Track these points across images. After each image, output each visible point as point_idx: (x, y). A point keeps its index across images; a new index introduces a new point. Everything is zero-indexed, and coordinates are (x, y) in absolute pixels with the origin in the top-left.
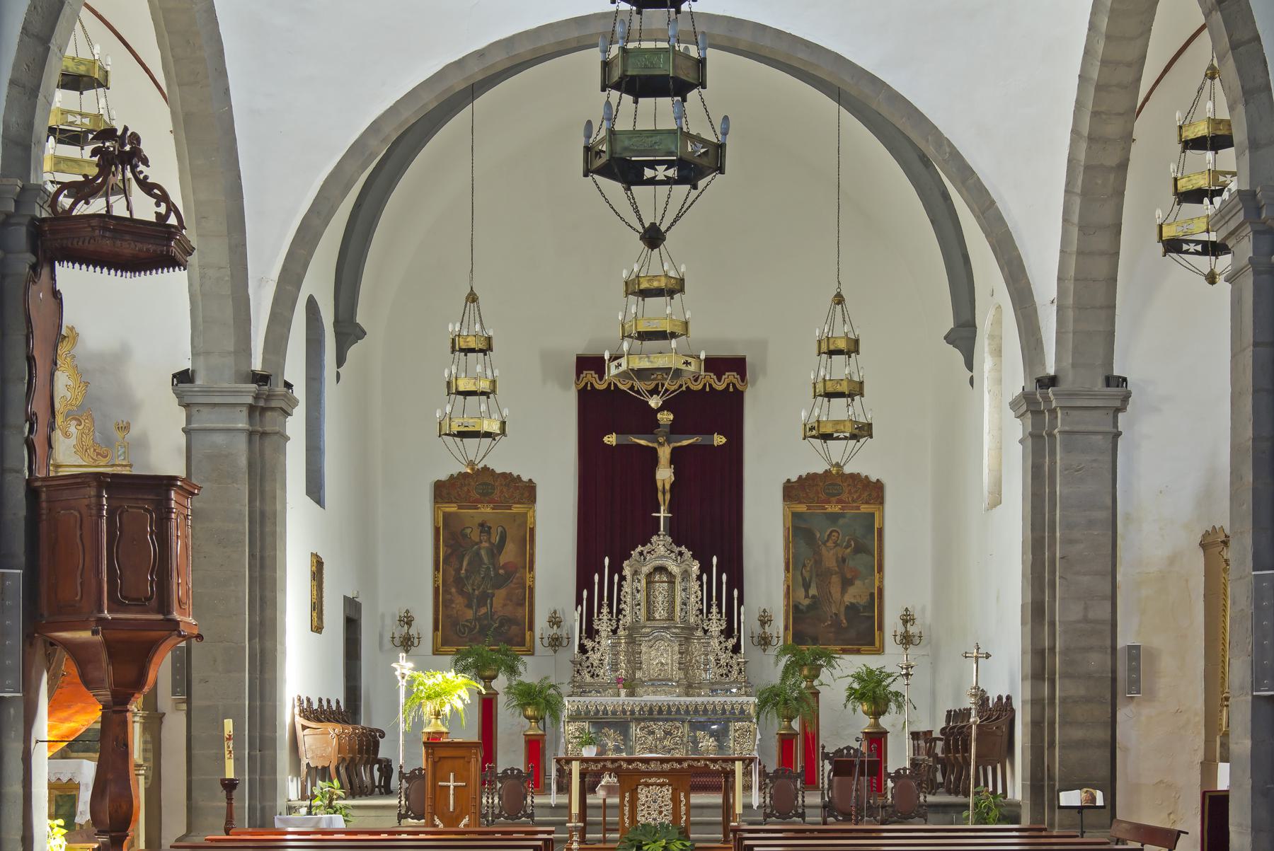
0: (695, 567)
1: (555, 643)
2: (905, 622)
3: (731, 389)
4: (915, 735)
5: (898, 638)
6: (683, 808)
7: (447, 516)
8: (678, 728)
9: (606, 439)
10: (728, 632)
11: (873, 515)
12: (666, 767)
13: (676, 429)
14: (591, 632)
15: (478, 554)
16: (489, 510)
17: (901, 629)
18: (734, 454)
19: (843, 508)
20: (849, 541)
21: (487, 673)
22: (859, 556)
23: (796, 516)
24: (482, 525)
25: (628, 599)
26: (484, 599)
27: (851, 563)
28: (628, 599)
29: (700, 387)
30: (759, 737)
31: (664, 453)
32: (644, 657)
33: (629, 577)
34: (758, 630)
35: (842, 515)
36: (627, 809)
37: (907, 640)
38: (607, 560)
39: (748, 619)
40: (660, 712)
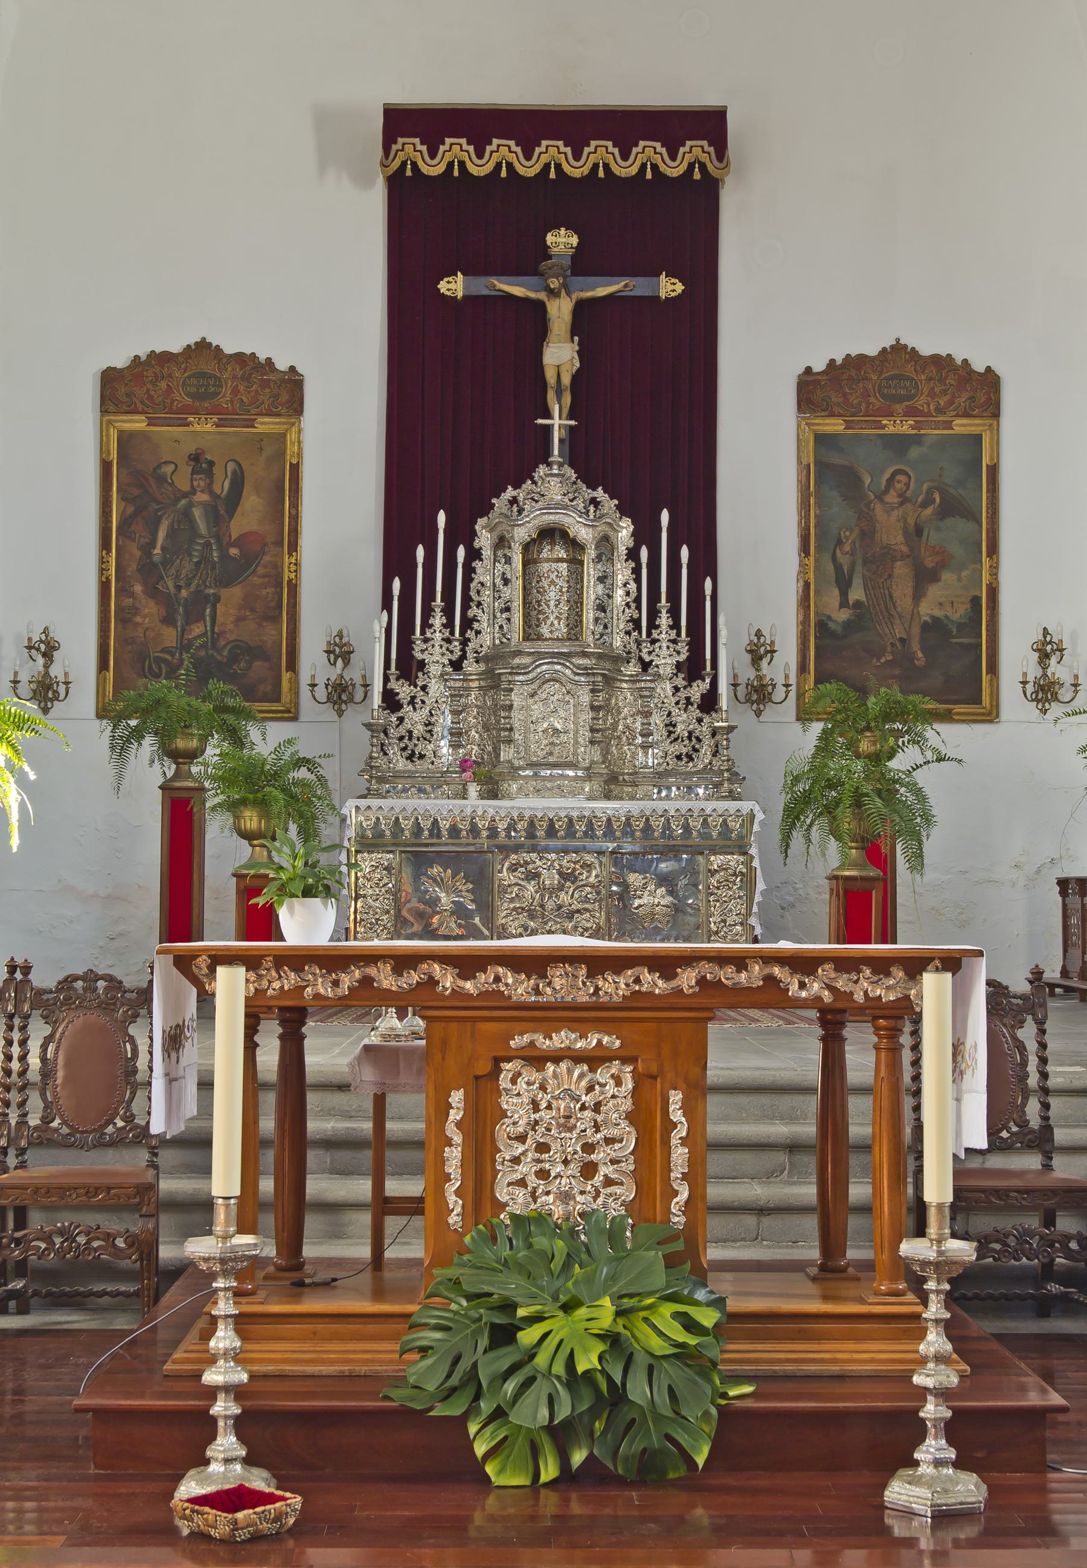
0: (625, 531)
1: (340, 695)
2: (1044, 657)
3: (697, 175)
4: (1063, 884)
5: (1030, 688)
6: (679, 1155)
7: (126, 440)
8: (588, 867)
9: (443, 286)
10: (693, 667)
11: (977, 439)
12: (614, 987)
13: (583, 264)
14: (408, 666)
15: (187, 514)
16: (209, 427)
17: (1034, 672)
18: (695, 323)
19: (917, 426)
20: (930, 491)
21: (181, 744)
22: (950, 521)
23: (822, 440)
24: (196, 458)
26: (200, 605)
27: (933, 537)
28: (487, 596)
29: (634, 170)
30: (761, 886)
32: (517, 717)
33: (487, 553)
34: (748, 674)
35: (916, 440)
36: (454, 1156)
37: (1045, 692)
38: (442, 518)
39: (729, 662)
40: (551, 832)
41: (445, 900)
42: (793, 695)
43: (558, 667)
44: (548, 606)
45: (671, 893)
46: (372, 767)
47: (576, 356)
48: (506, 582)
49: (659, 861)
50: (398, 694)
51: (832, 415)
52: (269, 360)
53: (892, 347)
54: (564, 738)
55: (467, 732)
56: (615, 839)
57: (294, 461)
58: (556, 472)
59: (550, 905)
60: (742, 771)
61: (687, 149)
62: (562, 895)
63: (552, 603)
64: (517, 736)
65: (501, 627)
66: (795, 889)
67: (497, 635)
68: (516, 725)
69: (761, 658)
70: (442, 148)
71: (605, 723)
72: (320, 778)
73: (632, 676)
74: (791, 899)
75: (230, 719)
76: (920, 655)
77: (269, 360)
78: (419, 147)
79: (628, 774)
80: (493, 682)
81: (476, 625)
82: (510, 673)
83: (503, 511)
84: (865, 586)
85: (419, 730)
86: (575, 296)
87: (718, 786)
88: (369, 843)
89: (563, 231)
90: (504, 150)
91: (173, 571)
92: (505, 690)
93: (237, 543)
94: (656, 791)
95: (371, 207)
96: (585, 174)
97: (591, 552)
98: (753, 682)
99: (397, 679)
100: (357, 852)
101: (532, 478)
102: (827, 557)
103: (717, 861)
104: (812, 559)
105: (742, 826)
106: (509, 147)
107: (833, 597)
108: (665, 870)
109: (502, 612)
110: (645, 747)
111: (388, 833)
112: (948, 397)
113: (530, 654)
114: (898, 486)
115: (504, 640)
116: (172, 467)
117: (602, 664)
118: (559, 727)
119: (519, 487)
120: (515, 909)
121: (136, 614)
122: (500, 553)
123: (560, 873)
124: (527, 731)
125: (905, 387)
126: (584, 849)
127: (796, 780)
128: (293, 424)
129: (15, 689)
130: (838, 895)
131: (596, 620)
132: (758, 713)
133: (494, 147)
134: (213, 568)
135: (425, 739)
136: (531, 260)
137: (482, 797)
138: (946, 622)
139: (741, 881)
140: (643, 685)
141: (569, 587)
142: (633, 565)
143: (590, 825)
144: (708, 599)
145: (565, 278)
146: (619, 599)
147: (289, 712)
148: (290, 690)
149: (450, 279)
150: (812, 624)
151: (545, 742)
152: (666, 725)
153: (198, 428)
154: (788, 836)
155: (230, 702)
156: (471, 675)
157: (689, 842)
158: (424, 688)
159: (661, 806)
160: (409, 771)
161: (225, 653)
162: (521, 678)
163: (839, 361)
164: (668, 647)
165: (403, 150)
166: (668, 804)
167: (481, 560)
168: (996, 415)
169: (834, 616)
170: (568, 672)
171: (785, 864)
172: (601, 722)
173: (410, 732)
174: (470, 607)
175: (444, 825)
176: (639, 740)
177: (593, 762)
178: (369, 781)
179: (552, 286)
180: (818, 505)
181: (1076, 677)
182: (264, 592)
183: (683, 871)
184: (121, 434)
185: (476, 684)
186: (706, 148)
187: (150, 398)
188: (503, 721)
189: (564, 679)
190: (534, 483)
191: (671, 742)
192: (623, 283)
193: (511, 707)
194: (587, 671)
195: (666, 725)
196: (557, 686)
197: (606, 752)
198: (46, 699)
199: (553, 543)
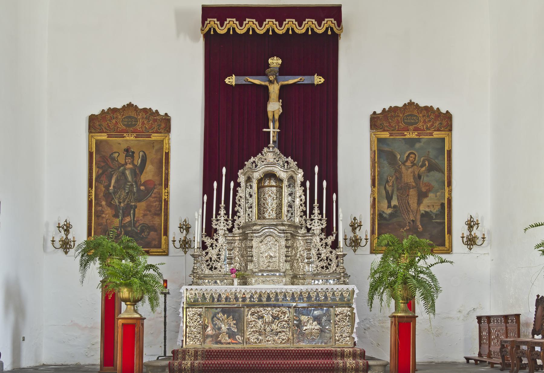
0: (300, 176)
1: (186, 244)
2: (470, 227)
3: (329, 33)
4: (479, 319)
5: (465, 240)
7: (99, 143)
8: (284, 313)
9: (227, 81)
10: (328, 230)
11: (443, 140)
13: (283, 71)
15: (123, 173)
17: (466, 233)
18: (329, 93)
19: (419, 135)
20: (424, 161)
22: (432, 173)
23: (380, 140)
24: (127, 150)
26: (128, 209)
27: (425, 179)
28: (243, 202)
29: (304, 31)
30: (357, 320)
31: (274, 89)
32: (255, 251)
33: (243, 184)
34: (350, 235)
35: (418, 140)
37: (471, 242)
38: (224, 170)
39: (343, 229)
41: (224, 328)
42: (369, 243)
43: (272, 230)
44: (268, 205)
45: (319, 324)
46: (194, 273)
47: (281, 108)
49: (314, 310)
51: (384, 131)
52: (157, 111)
53: (408, 103)
54: (274, 259)
57: (167, 151)
59: (268, 329)
60: (348, 272)
62: (273, 325)
63: (270, 204)
65: (249, 215)
66: (370, 322)
69: (356, 229)
70: (226, 23)
72: (159, 274)
74: (368, 326)
75: (131, 251)
76: (420, 227)
77: (157, 111)
78: (216, 22)
80: (245, 237)
81: (238, 214)
82: (252, 233)
84: (398, 199)
85: (215, 257)
87: (339, 279)
88: (191, 305)
90: (251, 23)
91: (118, 196)
93: (143, 184)
95: (198, 49)
97: (286, 183)
99: (206, 237)
102: (382, 188)
103: (339, 310)
104: (376, 188)
105: (349, 295)
107: (385, 204)
109: (249, 208)
110: (308, 263)
111: (200, 300)
112: (431, 123)
113: (260, 225)
114: (411, 159)
116: (118, 154)
118: (272, 255)
120: (253, 331)
121: (102, 214)
122: (248, 184)
123: (272, 316)
124: (259, 257)
125: (414, 119)
126: (282, 306)
128: (166, 136)
129: (53, 244)
130: (395, 325)
131: (288, 211)
132: (355, 251)
133: (247, 22)
134: (134, 195)
136: (261, 69)
137: (240, 284)
138: (431, 213)
140: (307, 238)
141: (277, 197)
142: (303, 188)
143: (285, 296)
144: (334, 202)
145: (276, 76)
146: (298, 203)
147: (165, 252)
149: (230, 78)
151: (266, 261)
153: (128, 138)
155: (131, 244)
157: (327, 302)
158: (217, 240)
161: (139, 229)
162: (257, 235)
163: (387, 109)
166: (318, 285)
167: (240, 187)
168: (451, 130)
169: (385, 211)
170: (276, 232)
171: (371, 311)
173: (211, 258)
175: (224, 296)
177: (286, 270)
180: (379, 167)
181: (484, 235)
182: (154, 204)
183: (324, 315)
184: (97, 141)
185: (238, 238)
186: (333, 22)
187: (109, 126)
189: (274, 235)
190: (262, 155)
193: (252, 247)
194: (284, 232)
196: (271, 238)
197: (292, 266)
198: (66, 248)
199: (270, 179)
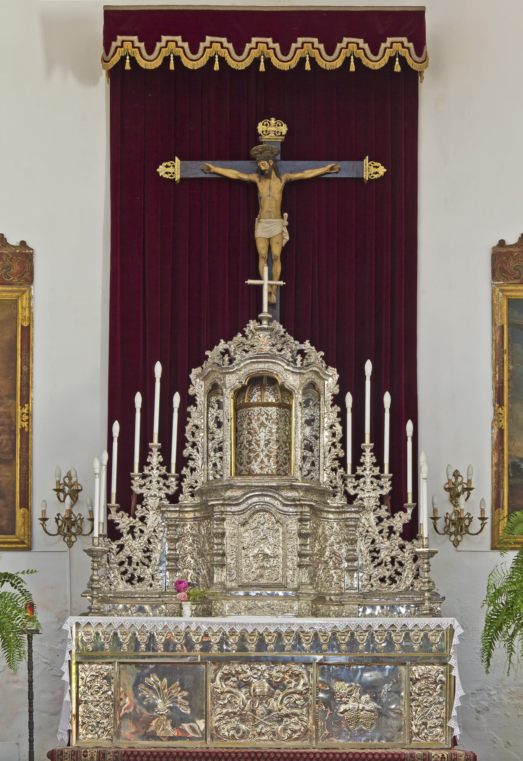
0: (331, 381)
1: (70, 527)
3: (397, 68)
8: (297, 676)
9: (162, 170)
10: (395, 501)
13: (292, 149)
14: (126, 499)
23: (512, 303)
25: (201, 437)
28: (201, 437)
30: (459, 692)
31: (271, 191)
33: (201, 399)
34: (446, 509)
39: (429, 497)
40: (261, 645)
43: (267, 499)
44: (259, 445)
45: (375, 699)
46: (93, 589)
47: (286, 230)
48: (219, 425)
49: (363, 671)
50: (118, 524)
55: (183, 558)
56: (322, 652)
57: (26, 324)
58: (266, 326)
59: (261, 710)
61: (388, 44)
62: (272, 701)
63: (262, 443)
64: (229, 560)
65: (215, 465)
66: (490, 696)
67: (211, 472)
68: (228, 550)
69: (458, 495)
70: (158, 45)
71: (312, 548)
72: (24, 592)
73: (338, 507)
74: (485, 704)
79: (335, 595)
81: (191, 463)
82: (222, 505)
83: (216, 361)
86: (284, 178)
87: (418, 605)
89: (273, 121)
90: (217, 47)
92: (217, 520)
94: (361, 610)
96: (292, 67)
97: (298, 398)
98: (451, 516)
99: (118, 511)
100: (78, 663)
101: (243, 333)
103: (418, 670)
104: (505, 408)
105: (441, 640)
106: (221, 43)
108: (369, 679)
109: (215, 451)
110: (351, 571)
111: (107, 646)
115: (218, 477)
117: (310, 497)
119: (231, 339)
120: (227, 714)
122: (213, 399)
123: (269, 682)
124: (238, 556)
127: (499, 593)
128: (24, 292)
131: (304, 458)
132: (456, 544)
133: (207, 44)
135: (144, 564)
136: (241, 145)
137: (196, 614)
139: (441, 688)
140: (348, 515)
141: (278, 429)
142: (339, 409)
145: (275, 161)
146: (326, 440)
147: (23, 543)
148: (24, 524)
149: (169, 164)
150: (506, 466)
151: (255, 566)
152: (371, 552)
154: (491, 646)
156: (186, 507)
157: (392, 654)
159: (365, 622)
160: (129, 592)
162: (234, 509)
164: (372, 483)
165: (122, 47)
167: (196, 405)
171: (487, 672)
172: (308, 548)
173: (130, 558)
174: (186, 447)
175: (160, 639)
176: (345, 565)
178: (91, 602)
179: (263, 168)
180: (512, 361)
183: (387, 680)
186: (406, 44)
188: (216, 547)
189: (273, 510)
190: (244, 335)
191: (375, 567)
192: (329, 166)
193: (223, 535)
194: (295, 502)
195: (371, 552)
196: (267, 515)
197: (313, 576)
199: (263, 389)
